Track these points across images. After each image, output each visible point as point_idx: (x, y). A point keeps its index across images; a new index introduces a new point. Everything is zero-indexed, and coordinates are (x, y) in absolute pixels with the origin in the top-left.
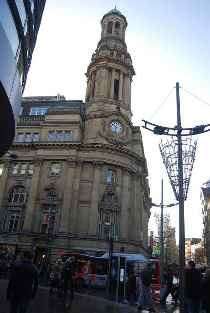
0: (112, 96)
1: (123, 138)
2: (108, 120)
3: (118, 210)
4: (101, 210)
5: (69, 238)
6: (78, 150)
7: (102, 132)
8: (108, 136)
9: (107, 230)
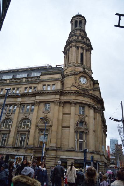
0: (80, 62)
1: (88, 87)
2: (78, 76)
3: (87, 131)
4: (76, 132)
5: (57, 151)
6: (61, 95)
7: (74, 84)
8: (78, 85)
9: (81, 144)
